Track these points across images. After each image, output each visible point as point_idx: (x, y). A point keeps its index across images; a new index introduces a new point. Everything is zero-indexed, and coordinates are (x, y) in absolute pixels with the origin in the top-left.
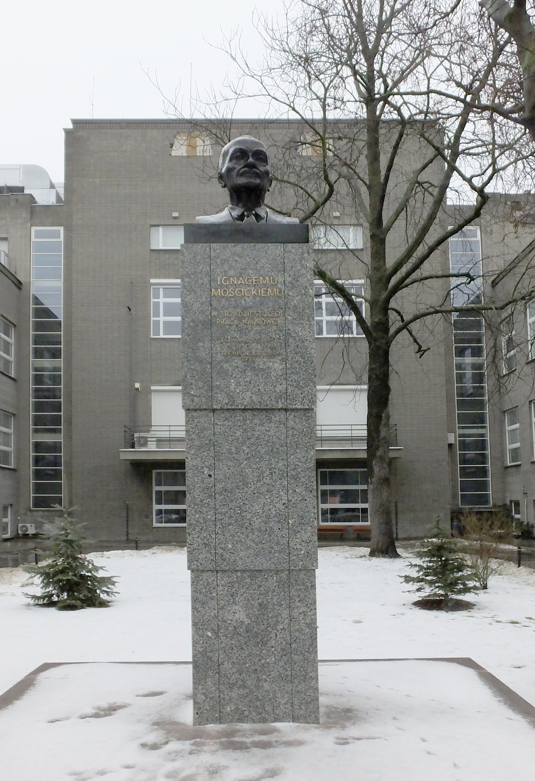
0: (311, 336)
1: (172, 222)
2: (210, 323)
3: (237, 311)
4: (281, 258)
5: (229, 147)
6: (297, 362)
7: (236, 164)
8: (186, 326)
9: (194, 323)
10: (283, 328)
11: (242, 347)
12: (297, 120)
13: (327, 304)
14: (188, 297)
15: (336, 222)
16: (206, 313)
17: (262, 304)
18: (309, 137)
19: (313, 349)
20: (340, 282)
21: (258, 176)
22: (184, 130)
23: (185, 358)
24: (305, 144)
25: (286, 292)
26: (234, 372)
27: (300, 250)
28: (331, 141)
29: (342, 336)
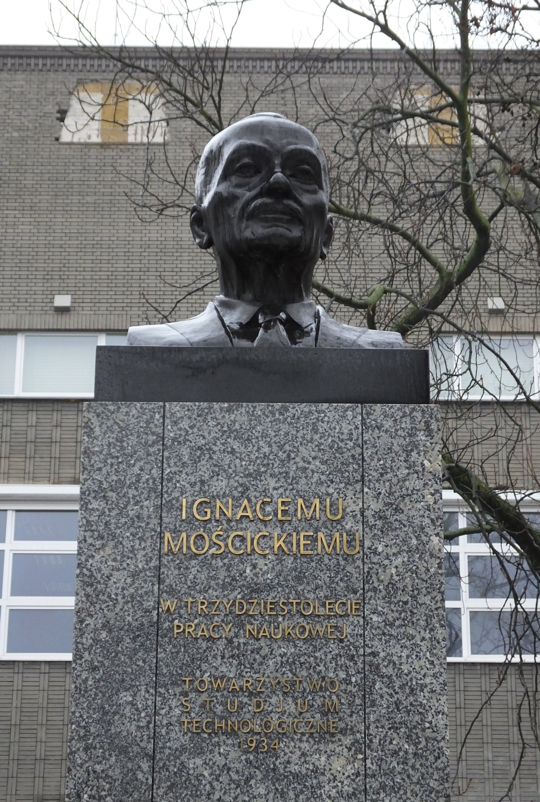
0: (434, 676)
1: (52, 321)
2: (154, 632)
3: (231, 597)
4: (356, 445)
5: (223, 141)
6: (395, 753)
7: (238, 186)
8: (87, 640)
9: (110, 631)
10: (356, 648)
11: (242, 706)
12: (394, 52)
13: (473, 560)
14: (97, 557)
15: (494, 325)
16: (146, 605)
17: (299, 579)
18: (423, 98)
19: (442, 715)
20: (510, 497)
21: (294, 218)
22: (97, 76)
23: (81, 739)
24: (413, 116)
25: (367, 543)
26: (215, 783)
27: (406, 423)
28: (480, 110)
29: (516, 659)
